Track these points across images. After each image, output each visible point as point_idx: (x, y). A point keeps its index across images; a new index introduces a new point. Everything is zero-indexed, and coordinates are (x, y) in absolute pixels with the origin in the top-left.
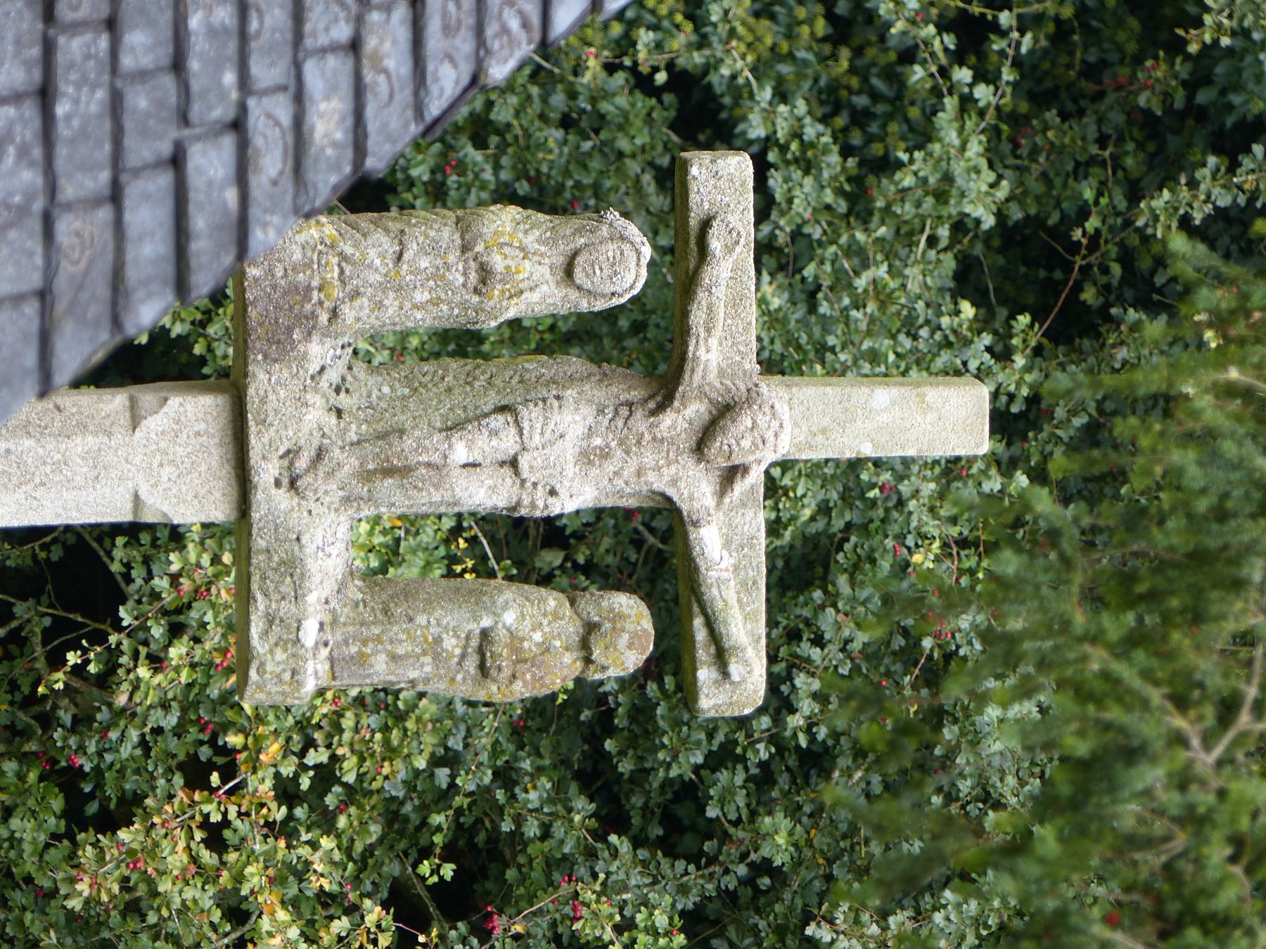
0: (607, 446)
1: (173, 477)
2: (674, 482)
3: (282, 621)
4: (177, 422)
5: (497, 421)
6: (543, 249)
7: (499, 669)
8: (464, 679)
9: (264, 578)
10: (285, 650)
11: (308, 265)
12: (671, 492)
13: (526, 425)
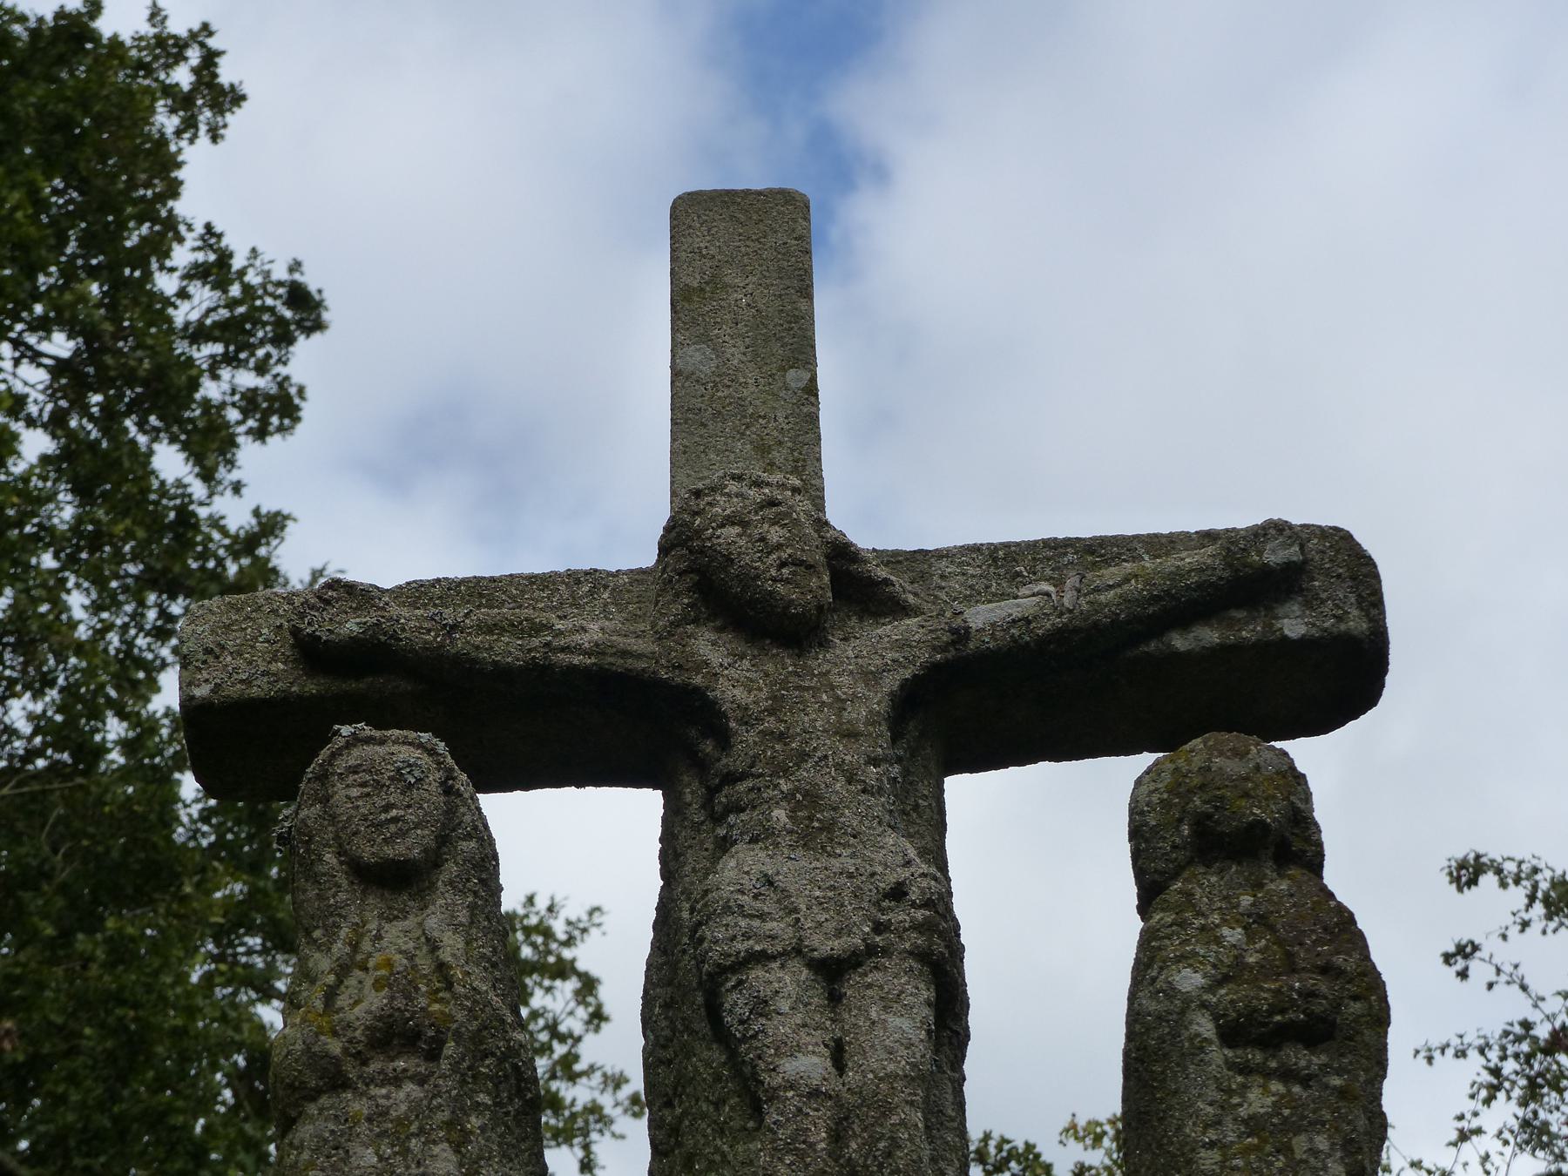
0: (788, 797)
2: (871, 677)
5: (736, 1003)
6: (344, 932)
7: (1309, 994)
8: (1339, 1072)
12: (891, 682)
13: (741, 946)
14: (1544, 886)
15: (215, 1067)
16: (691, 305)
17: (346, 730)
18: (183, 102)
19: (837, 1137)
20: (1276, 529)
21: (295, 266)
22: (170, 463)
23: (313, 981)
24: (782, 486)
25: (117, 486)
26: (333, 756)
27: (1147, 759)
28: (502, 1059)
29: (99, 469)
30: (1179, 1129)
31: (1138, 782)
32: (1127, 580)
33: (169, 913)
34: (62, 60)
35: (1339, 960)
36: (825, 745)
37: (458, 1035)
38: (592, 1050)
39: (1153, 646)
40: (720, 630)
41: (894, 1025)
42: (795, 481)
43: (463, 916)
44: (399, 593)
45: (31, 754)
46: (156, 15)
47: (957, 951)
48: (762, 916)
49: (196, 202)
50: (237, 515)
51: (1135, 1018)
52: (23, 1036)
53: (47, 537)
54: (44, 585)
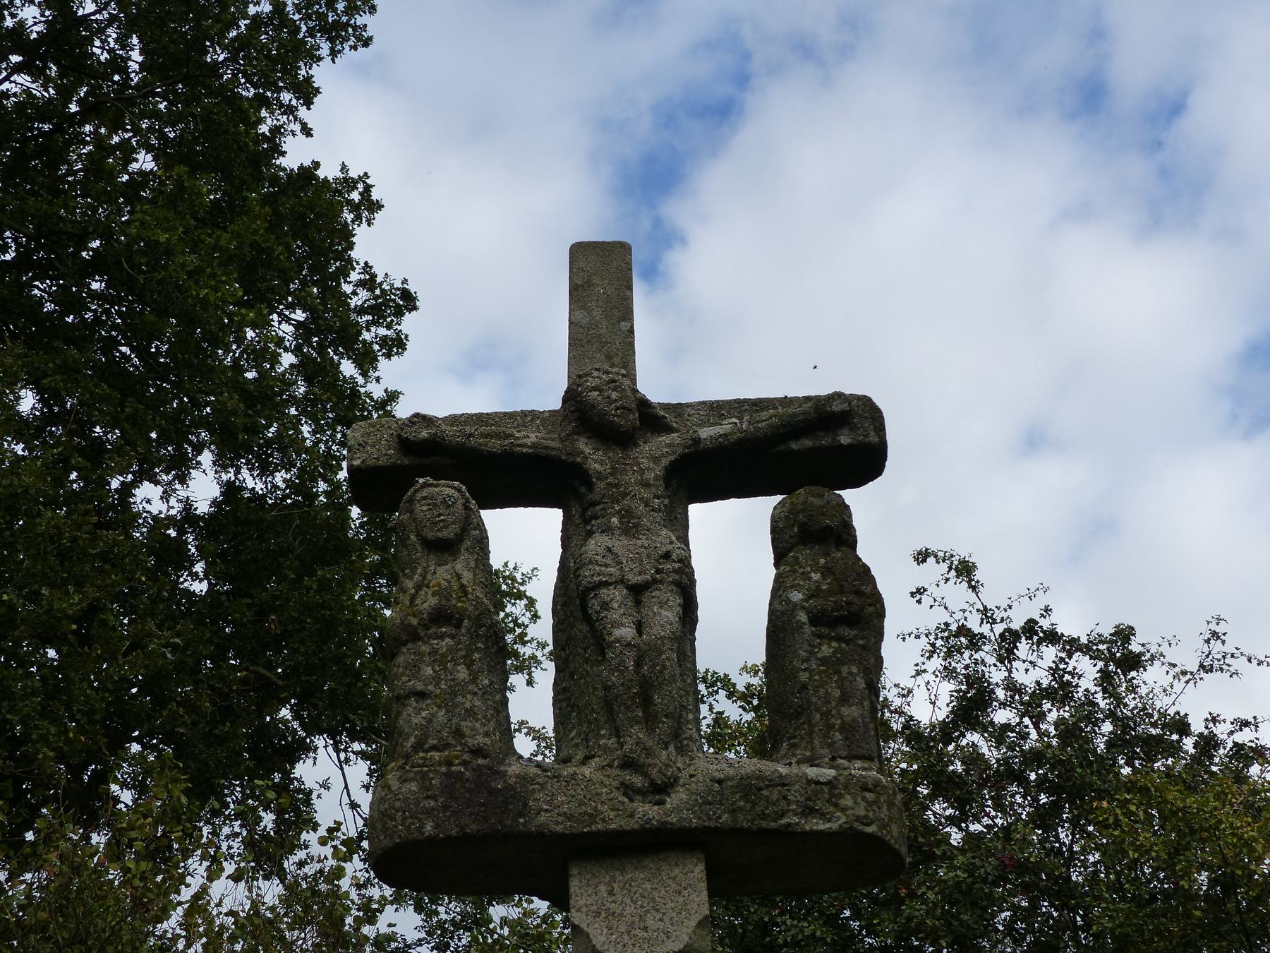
0: (618, 512)
1: (658, 916)
2: (656, 460)
3: (810, 799)
4: (598, 914)
5: (594, 604)
7: (849, 603)
9: (764, 816)
10: (841, 796)
11: (424, 776)
12: (665, 462)
13: (596, 579)
14: (956, 563)
15: (365, 637)
16: (578, 292)
17: (421, 480)
18: (355, 208)
19: (638, 664)
20: (838, 396)
21: (405, 281)
22: (348, 368)
23: (405, 592)
24: (617, 374)
25: (324, 378)
26: (416, 491)
27: (779, 498)
28: (490, 627)
29: (317, 371)
30: (791, 662)
31: (775, 508)
32: (771, 418)
33: (346, 568)
34: (301, 188)
35: (863, 588)
36: (636, 489)
37: (469, 617)
38: (532, 631)
39: (782, 447)
40: (589, 438)
41: (665, 616)
42: (624, 372)
43: (472, 564)
44: (445, 419)
45: (285, 497)
46: (344, 168)
47: (693, 582)
48: (606, 566)
49: (359, 253)
50: (377, 391)
51: (772, 612)
52: (280, 622)
53: (293, 400)
54: (291, 422)
